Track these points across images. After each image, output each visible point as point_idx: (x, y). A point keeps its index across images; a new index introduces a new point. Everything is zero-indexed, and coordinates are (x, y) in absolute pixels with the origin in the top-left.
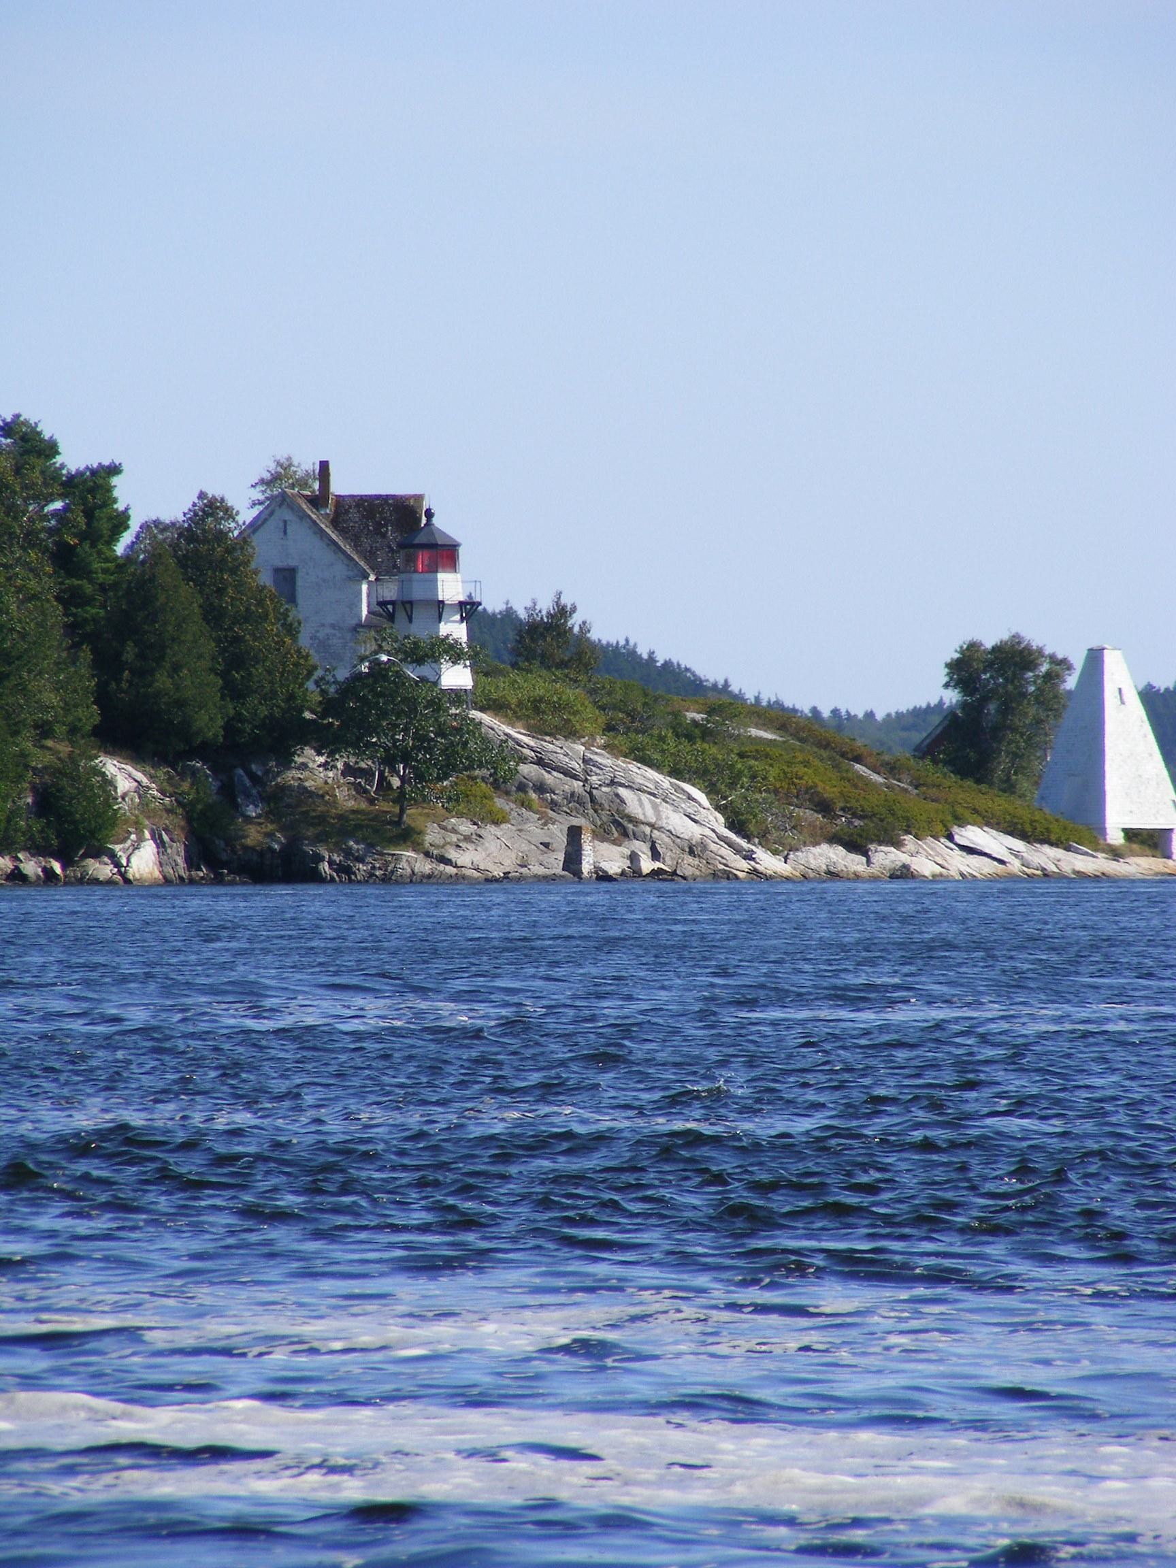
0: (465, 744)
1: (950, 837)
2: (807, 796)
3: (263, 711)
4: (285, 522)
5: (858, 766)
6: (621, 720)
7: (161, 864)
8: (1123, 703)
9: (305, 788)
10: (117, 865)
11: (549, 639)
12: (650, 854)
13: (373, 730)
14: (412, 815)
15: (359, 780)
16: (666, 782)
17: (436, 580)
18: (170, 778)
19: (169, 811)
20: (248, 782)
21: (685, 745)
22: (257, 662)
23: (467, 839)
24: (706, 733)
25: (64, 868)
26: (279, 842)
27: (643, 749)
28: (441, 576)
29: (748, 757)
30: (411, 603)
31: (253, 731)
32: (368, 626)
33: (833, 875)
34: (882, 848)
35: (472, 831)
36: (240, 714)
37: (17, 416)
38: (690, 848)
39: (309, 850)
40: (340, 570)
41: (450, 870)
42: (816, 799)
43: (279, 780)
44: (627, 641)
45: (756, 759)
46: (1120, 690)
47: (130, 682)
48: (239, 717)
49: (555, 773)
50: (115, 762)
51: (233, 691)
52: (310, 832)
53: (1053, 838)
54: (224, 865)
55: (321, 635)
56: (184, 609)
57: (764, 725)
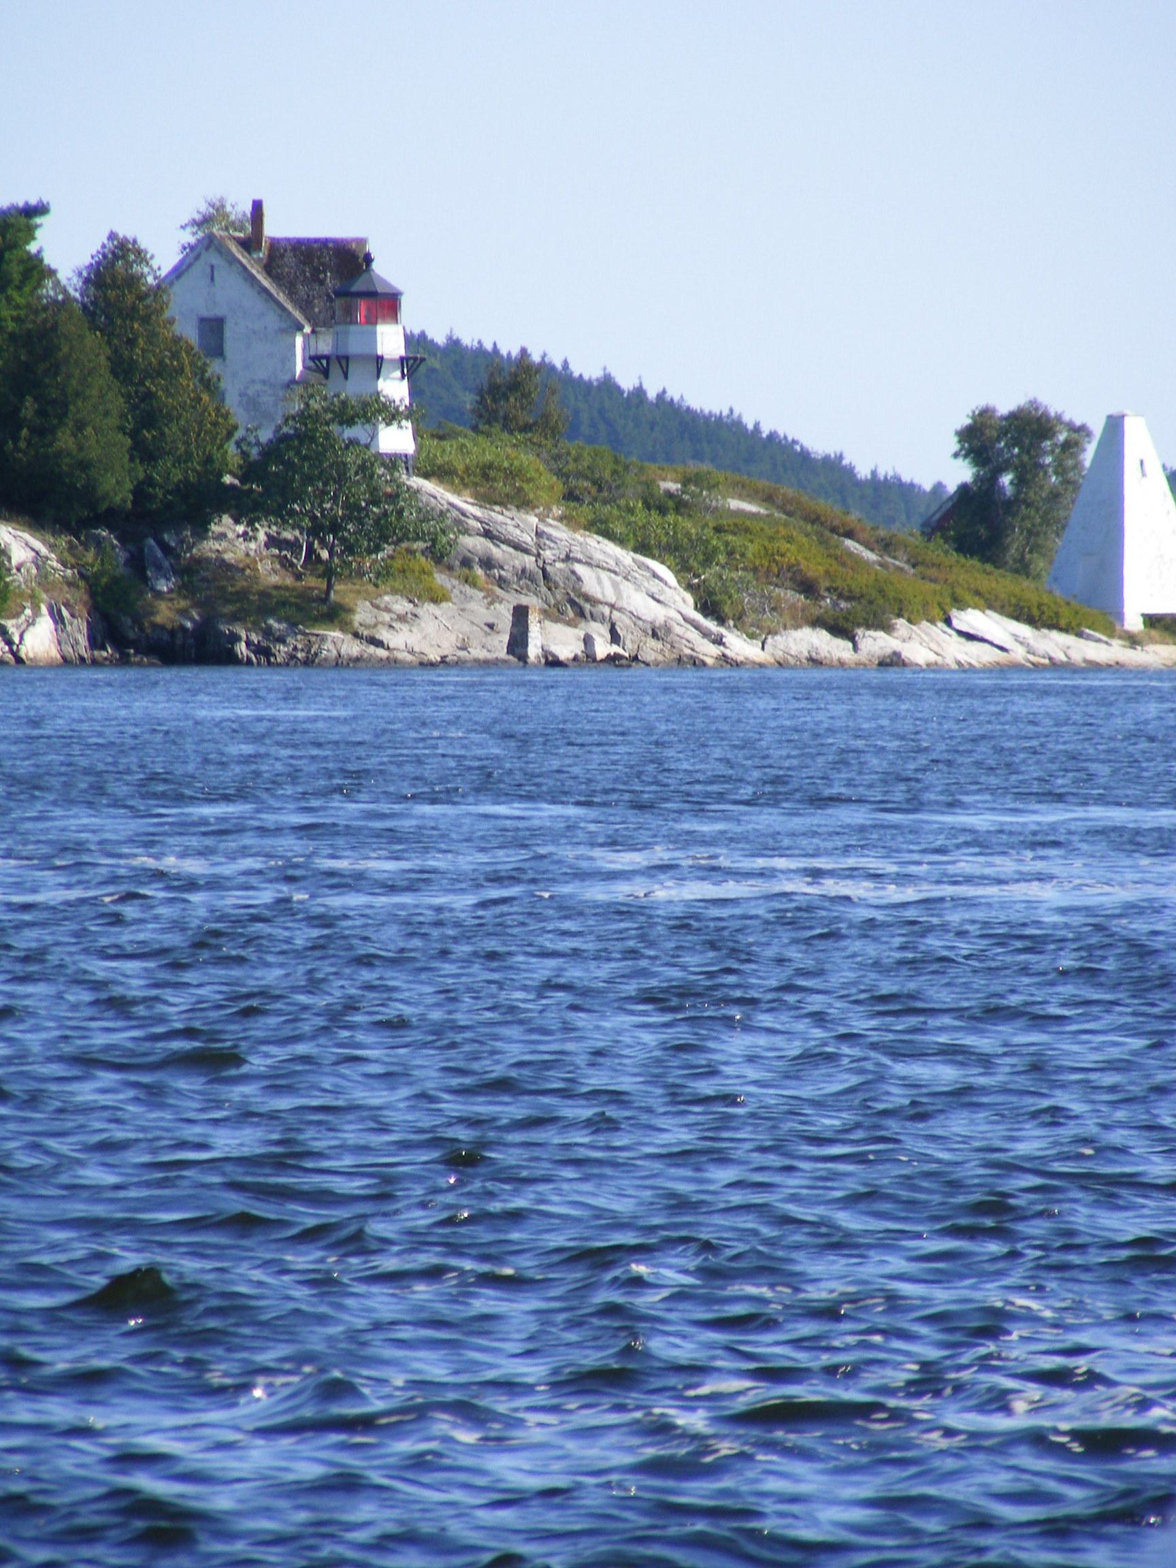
0: (400, 513)
1: (948, 621)
3: (177, 475)
4: (212, 267)
5: (849, 543)
6: (586, 489)
7: (59, 643)
8: (1144, 475)
9: (223, 560)
11: (512, 400)
12: (609, 637)
13: (299, 497)
14: (341, 591)
15: (284, 553)
16: (626, 557)
17: (375, 333)
18: (71, 548)
19: (70, 584)
20: (159, 554)
21: (655, 517)
22: (171, 420)
23: (402, 618)
24: (679, 505)
26: (192, 619)
27: (605, 522)
29: (725, 531)
30: (347, 358)
31: (165, 496)
32: (303, 382)
33: (815, 662)
34: (871, 633)
38: (653, 630)
39: (225, 628)
40: (272, 320)
41: (381, 653)
42: (798, 578)
43: (194, 551)
44: (731, 410)
45: (734, 534)
46: (1142, 462)
48: (149, 481)
49: (504, 547)
50: (10, 529)
51: (144, 452)
52: (228, 609)
53: (1063, 623)
54: (130, 644)
55: (250, 392)
56: (89, 361)
57: (748, 496)
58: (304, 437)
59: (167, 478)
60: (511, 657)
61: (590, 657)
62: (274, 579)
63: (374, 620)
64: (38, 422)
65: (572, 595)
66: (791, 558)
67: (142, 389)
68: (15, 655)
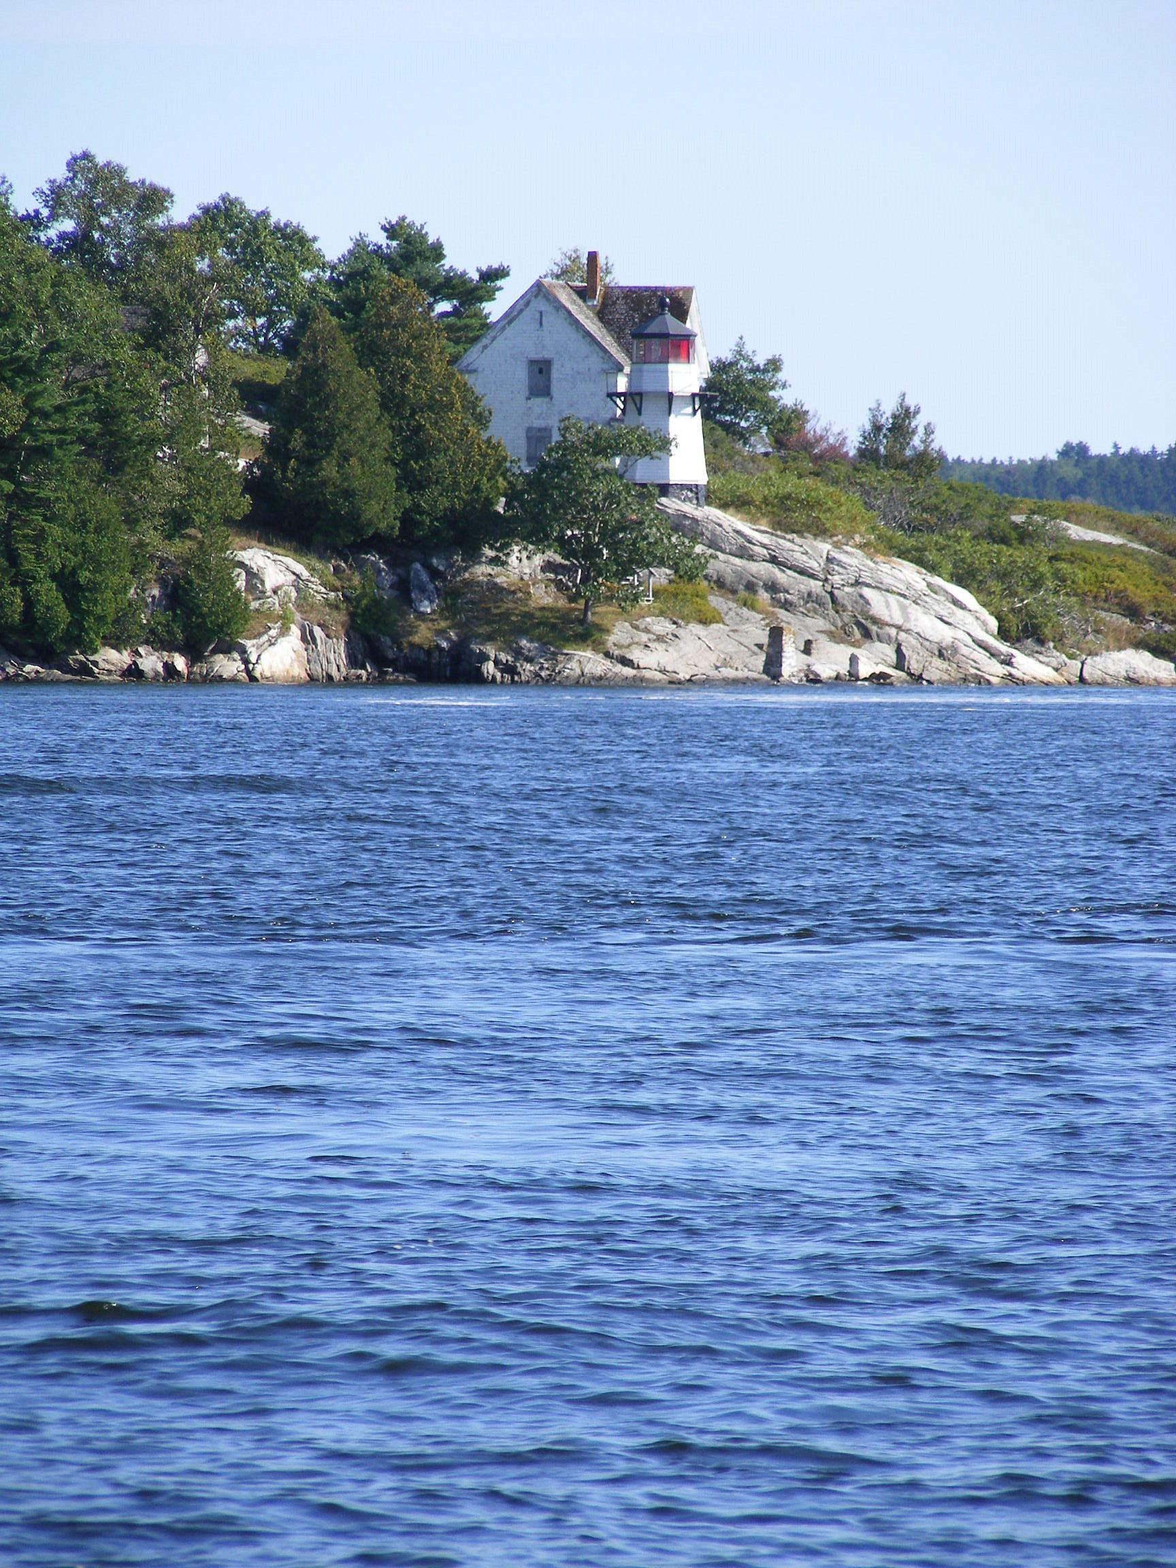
2: (1117, 600)
3: (444, 503)
9: (496, 584)
10: (246, 662)
19: (335, 607)
20: (424, 576)
22: (439, 452)
23: (660, 639)
25: (190, 665)
26: (449, 639)
28: (672, 367)
30: (640, 394)
31: (431, 521)
33: (1133, 681)
35: (669, 631)
36: (419, 506)
37: (403, 219)
39: (476, 648)
40: (596, 363)
41: (628, 671)
43: (467, 575)
47: (297, 472)
48: (416, 508)
49: (789, 572)
50: (269, 554)
51: (411, 482)
52: (484, 630)
58: (561, 466)
59: (433, 506)
60: (765, 677)
61: (853, 676)
62: (548, 601)
63: (628, 641)
64: (307, 453)
65: (860, 618)
66: (1119, 585)
67: (413, 423)
68: (248, 672)
